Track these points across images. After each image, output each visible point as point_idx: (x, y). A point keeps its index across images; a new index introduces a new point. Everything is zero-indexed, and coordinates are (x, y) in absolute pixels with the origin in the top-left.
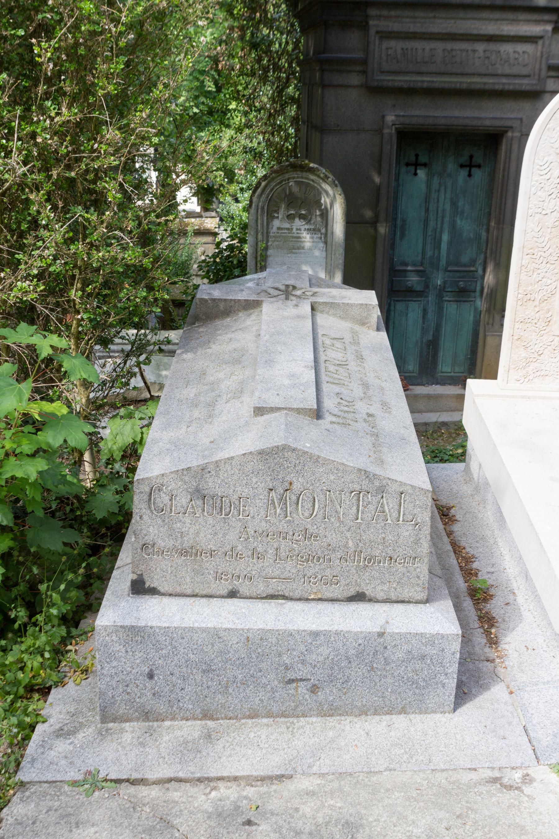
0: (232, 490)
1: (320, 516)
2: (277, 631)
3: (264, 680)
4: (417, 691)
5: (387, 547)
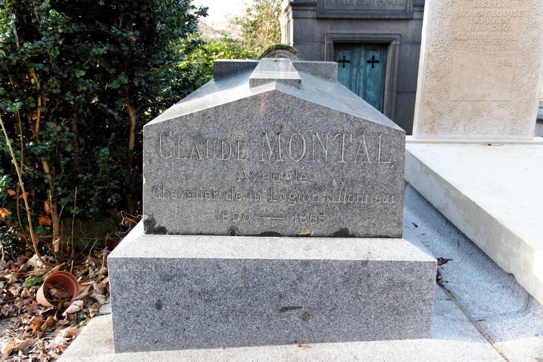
0: (229, 135)
1: (307, 157)
2: (271, 260)
3: (261, 309)
5: (366, 185)
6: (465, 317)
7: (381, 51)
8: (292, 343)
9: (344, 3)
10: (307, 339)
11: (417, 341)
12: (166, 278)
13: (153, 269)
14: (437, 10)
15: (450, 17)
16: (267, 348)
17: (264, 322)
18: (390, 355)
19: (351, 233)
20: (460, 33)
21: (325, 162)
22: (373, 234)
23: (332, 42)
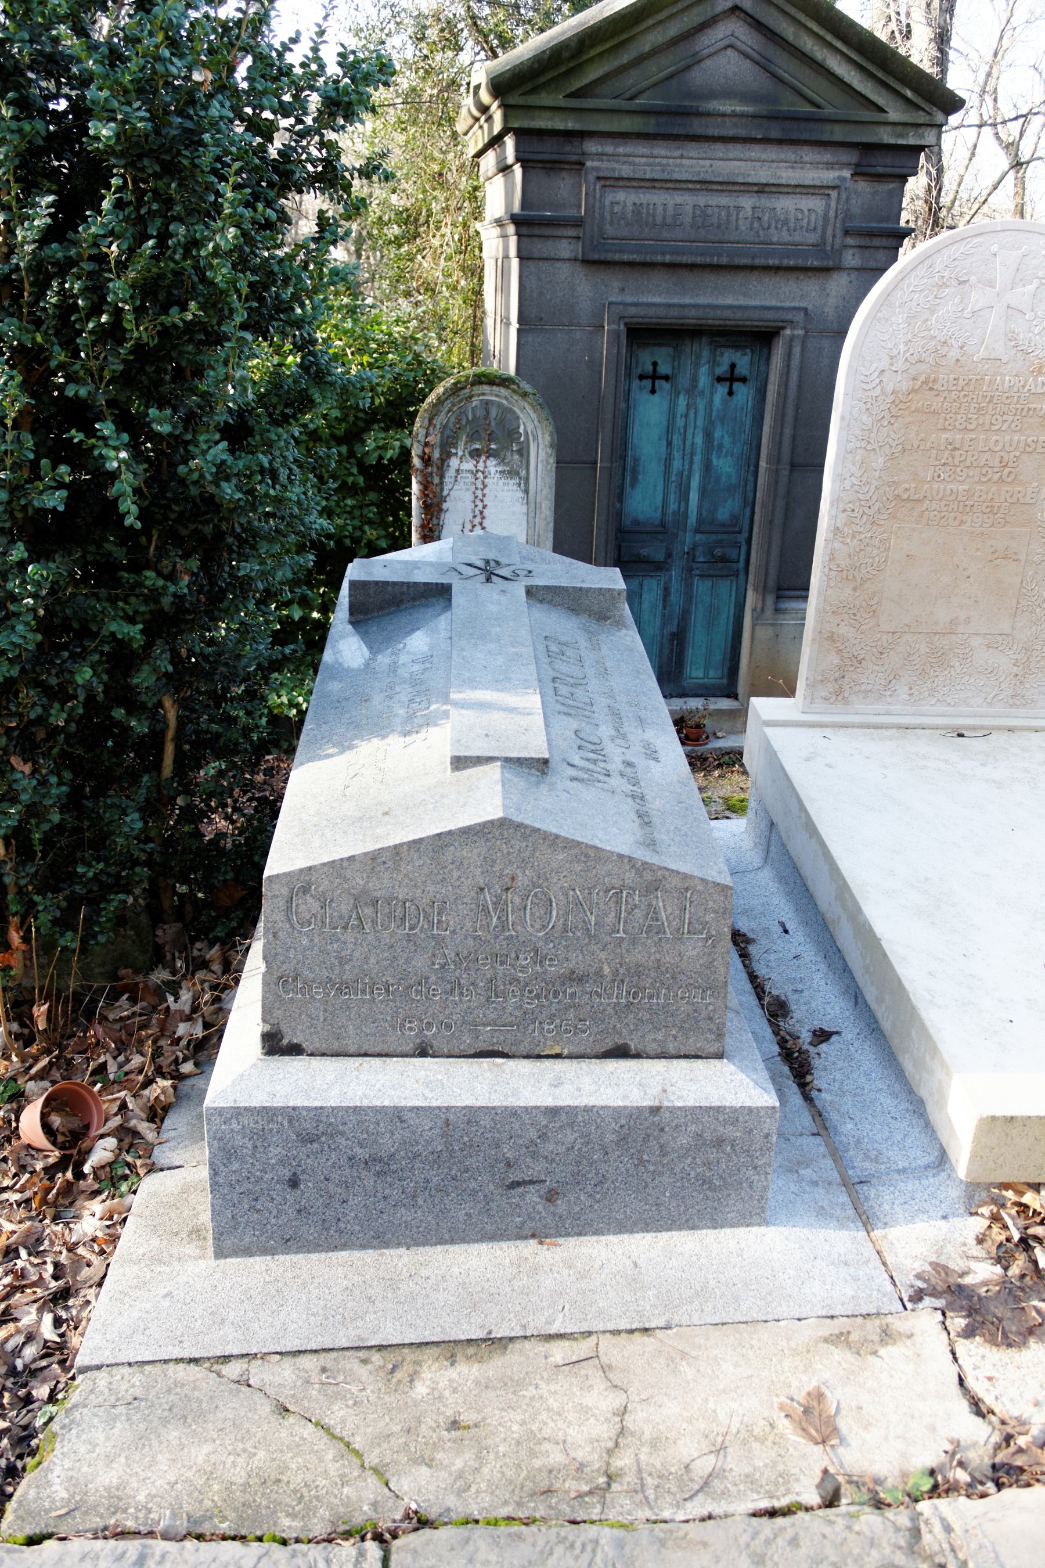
0: (419, 891)
2: (494, 1108)
3: (473, 1185)
4: (710, 1194)
5: (663, 973)
6: (836, 1174)
7: (753, 352)
8: (526, 1238)
9: (659, 220)
10: (553, 1231)
11: (741, 1232)
12: (308, 1139)
13: (285, 1123)
14: (858, 432)
15: (887, 449)
16: (484, 1247)
17: (479, 1206)
18: (694, 1258)
19: (633, 1052)
20: (907, 486)
21: (589, 936)
22: (673, 1052)
23: (622, 327)
